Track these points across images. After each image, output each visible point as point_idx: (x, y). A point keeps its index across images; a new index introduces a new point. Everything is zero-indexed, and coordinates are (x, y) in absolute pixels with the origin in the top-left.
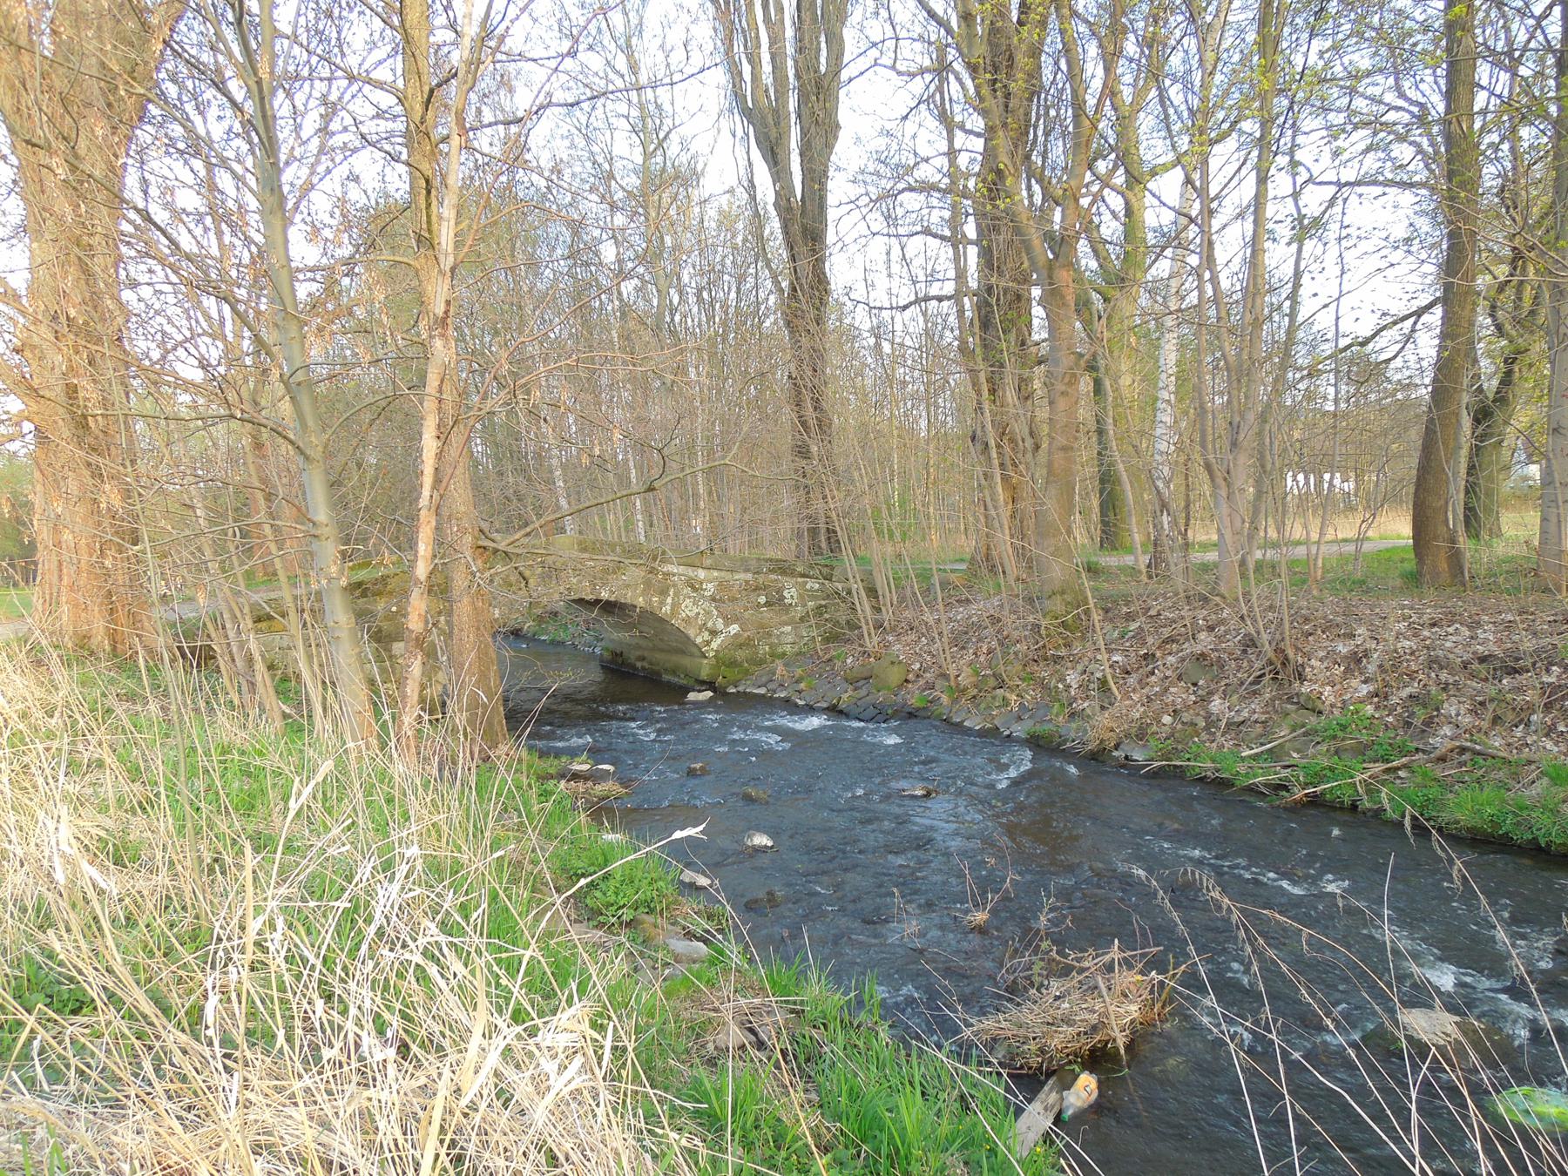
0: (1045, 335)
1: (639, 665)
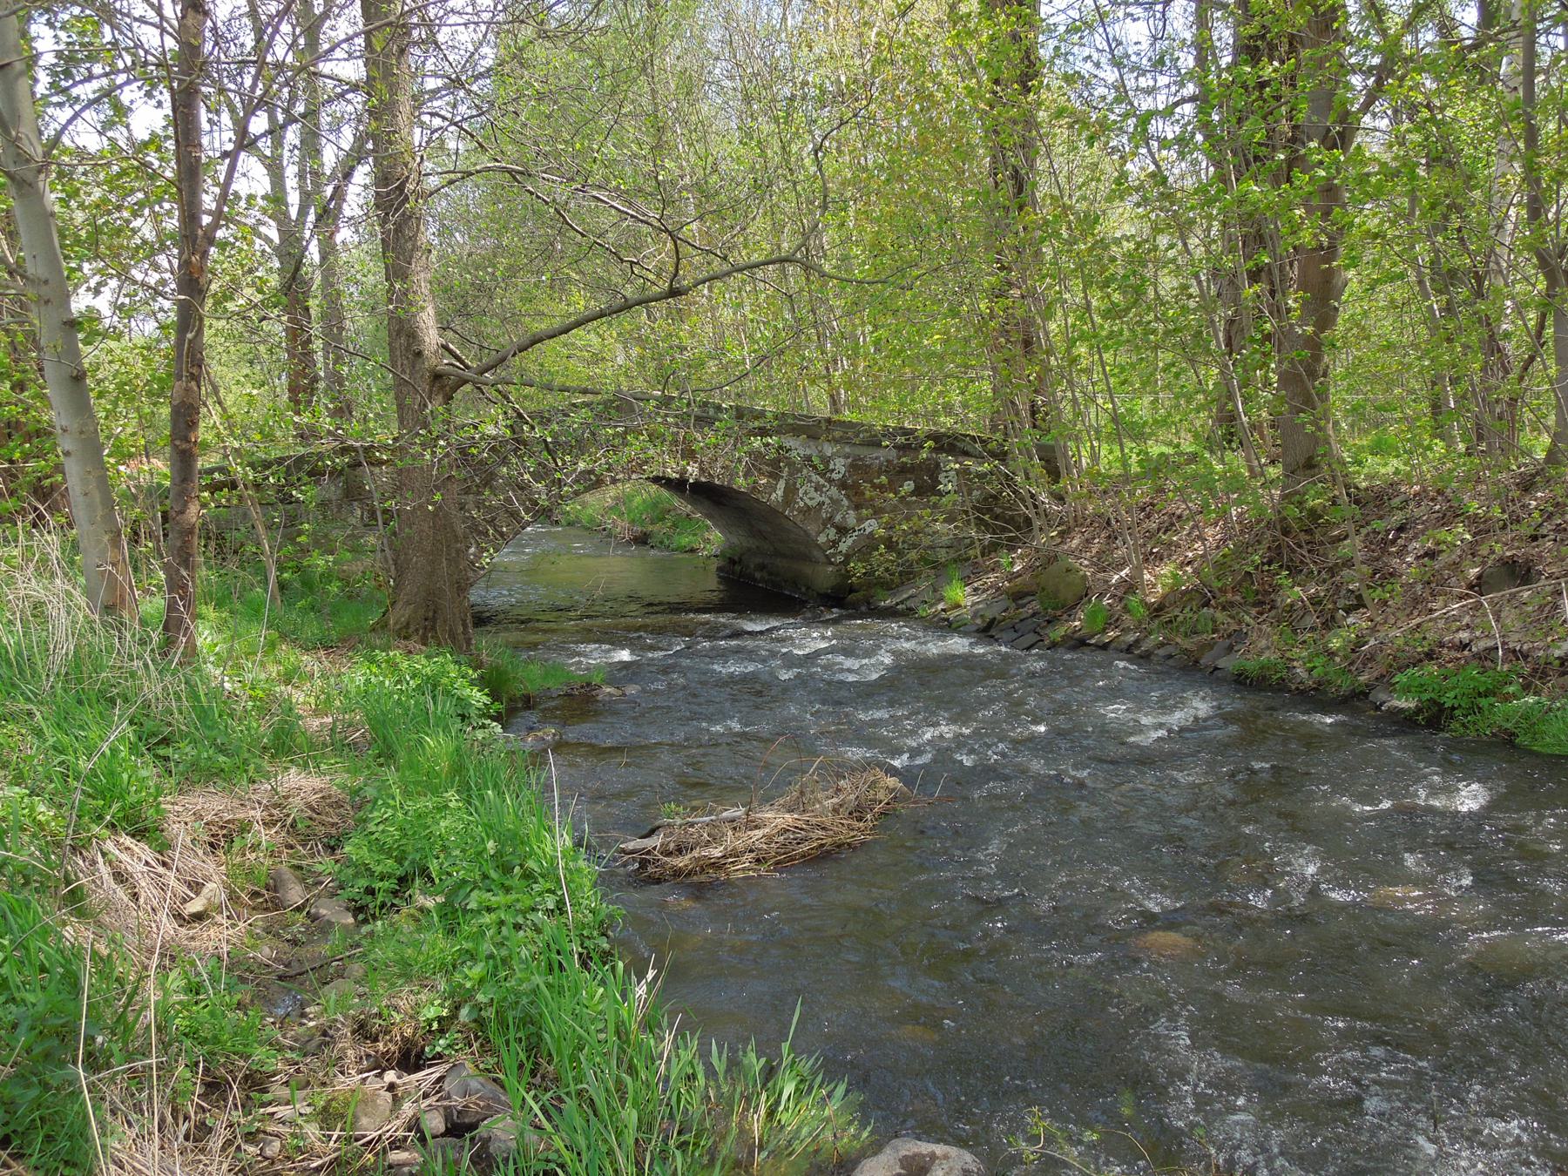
0: (354, 70)
1: (758, 575)
